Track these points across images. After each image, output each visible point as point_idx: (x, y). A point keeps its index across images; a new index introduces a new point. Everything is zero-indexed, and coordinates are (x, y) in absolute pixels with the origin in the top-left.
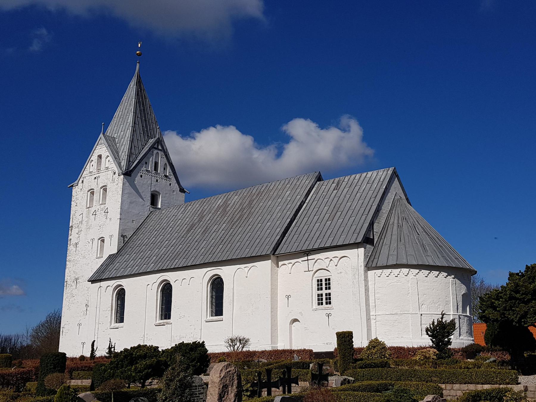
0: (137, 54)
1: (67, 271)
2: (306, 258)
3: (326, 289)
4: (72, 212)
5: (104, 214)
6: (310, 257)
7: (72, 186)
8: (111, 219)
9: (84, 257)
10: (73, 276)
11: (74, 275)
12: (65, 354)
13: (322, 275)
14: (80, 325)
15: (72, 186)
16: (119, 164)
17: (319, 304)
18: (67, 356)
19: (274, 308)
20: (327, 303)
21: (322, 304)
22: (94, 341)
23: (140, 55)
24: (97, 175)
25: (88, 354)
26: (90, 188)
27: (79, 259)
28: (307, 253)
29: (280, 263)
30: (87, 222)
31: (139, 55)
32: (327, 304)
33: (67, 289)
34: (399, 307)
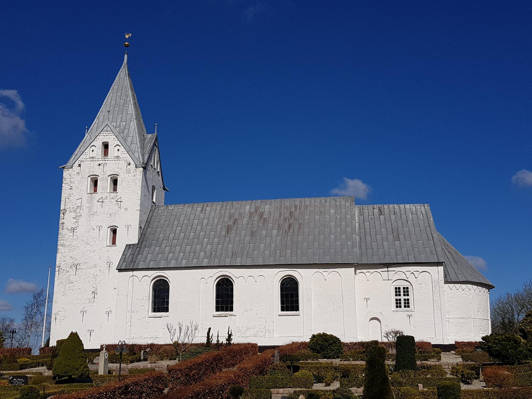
0: (125, 45)
1: (58, 256)
2: (386, 269)
3: (404, 295)
4: (64, 196)
5: (115, 203)
6: (389, 269)
7: (64, 168)
8: (126, 209)
9: (87, 243)
10: (70, 262)
11: (72, 261)
12: (413, 338)
13: (402, 284)
14: (83, 312)
15: (64, 168)
16: (143, 155)
17: (397, 307)
18: (416, 340)
19: (351, 307)
20: (405, 307)
21: (400, 307)
22: (210, 329)
23: (127, 47)
24: (104, 162)
25: (204, 341)
26: (92, 174)
27: (79, 245)
28: (388, 265)
29: (358, 271)
30: (90, 208)
31: (127, 46)
32: (405, 307)
33: (61, 276)
34: (451, 314)
